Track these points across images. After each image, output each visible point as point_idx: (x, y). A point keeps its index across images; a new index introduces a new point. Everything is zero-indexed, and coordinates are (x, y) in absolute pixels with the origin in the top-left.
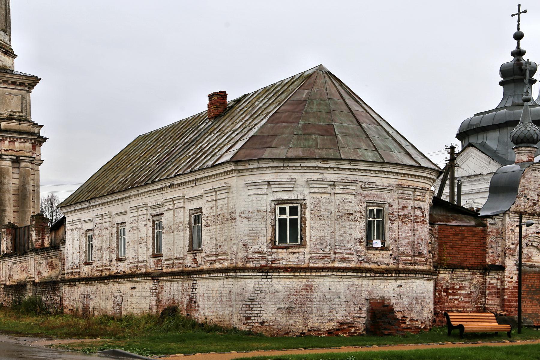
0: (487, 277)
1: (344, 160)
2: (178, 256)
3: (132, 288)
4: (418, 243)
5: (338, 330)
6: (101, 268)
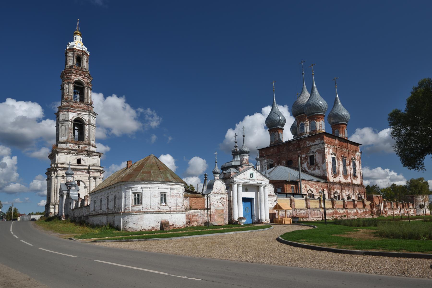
0: (205, 211)
1: (152, 181)
4: (178, 203)
5: (152, 229)
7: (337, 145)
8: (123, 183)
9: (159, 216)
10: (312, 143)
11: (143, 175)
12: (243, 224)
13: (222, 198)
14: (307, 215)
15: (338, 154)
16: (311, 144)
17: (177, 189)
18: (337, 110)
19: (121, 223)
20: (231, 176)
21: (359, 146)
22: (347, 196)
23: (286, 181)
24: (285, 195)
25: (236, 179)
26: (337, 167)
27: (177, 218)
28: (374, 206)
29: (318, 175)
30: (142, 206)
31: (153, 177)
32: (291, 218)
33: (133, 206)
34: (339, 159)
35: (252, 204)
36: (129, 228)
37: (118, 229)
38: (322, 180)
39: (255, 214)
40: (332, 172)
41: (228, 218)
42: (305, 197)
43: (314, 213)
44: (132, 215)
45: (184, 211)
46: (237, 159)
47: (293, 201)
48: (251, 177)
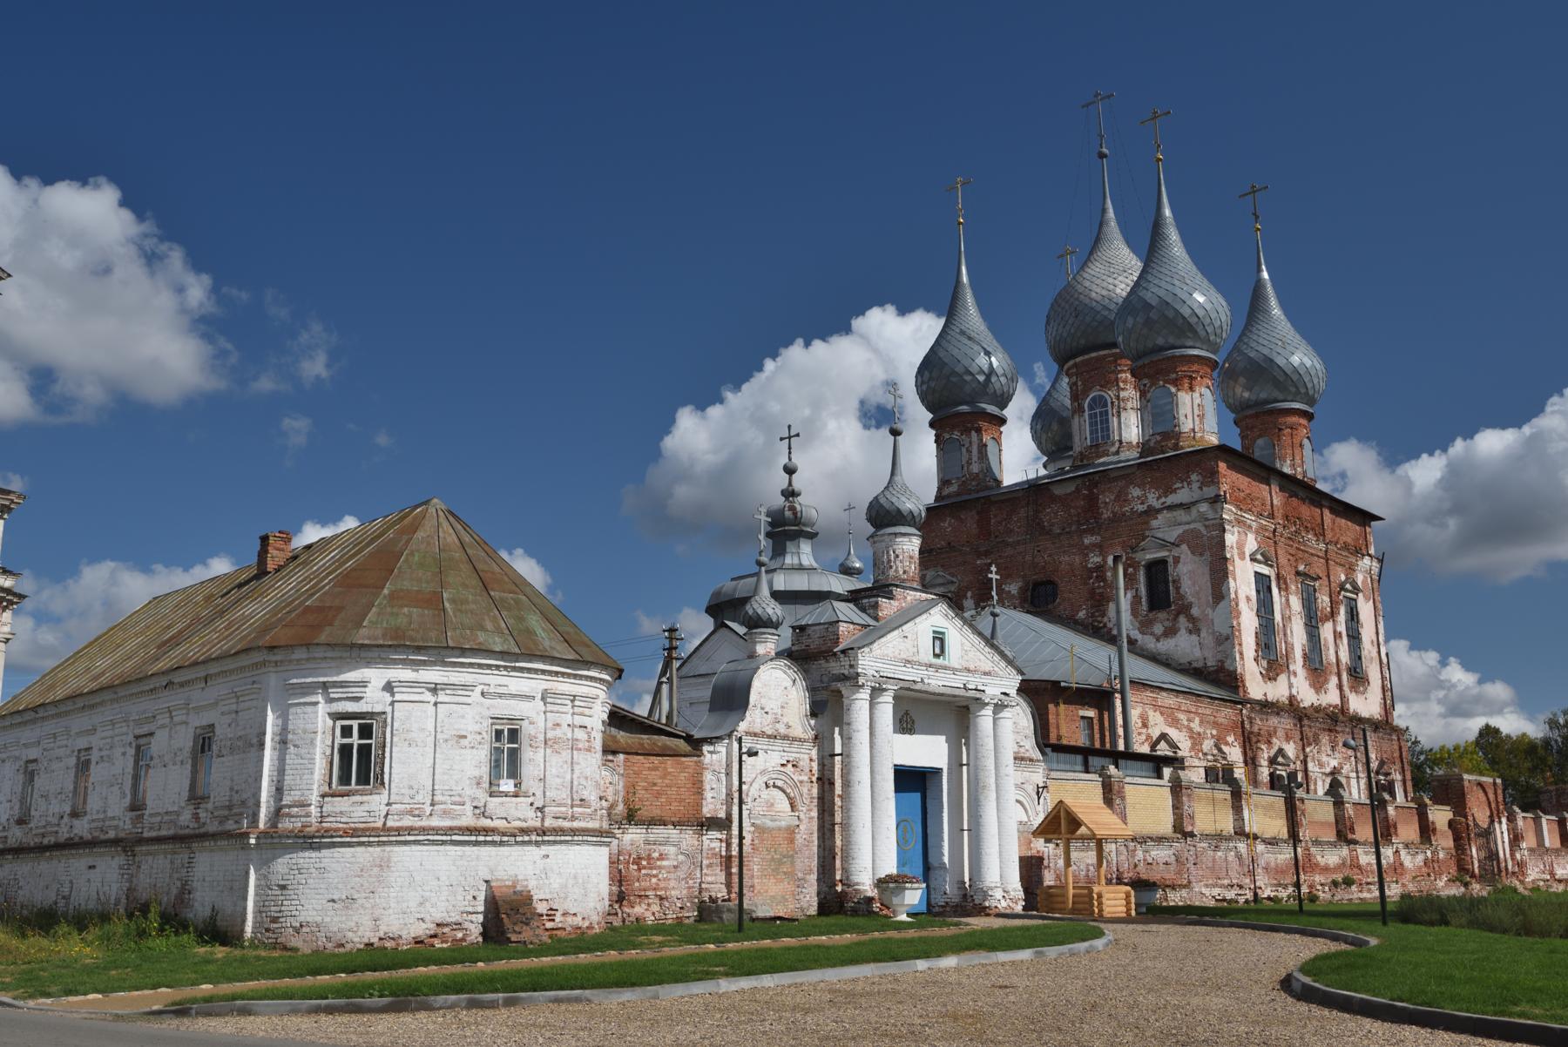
0: (704, 837)
1: (453, 648)
2: (170, 809)
3: (90, 867)
4: (579, 784)
5: (435, 936)
6: (43, 830)
7: (1279, 514)
8: (278, 658)
9: (478, 858)
10: (1158, 499)
11: (395, 610)
12: (908, 915)
13: (790, 765)
14: (1179, 873)
15: (1283, 560)
16: (1153, 499)
17: (577, 703)
18: (1265, 343)
19: (245, 899)
20: (837, 642)
21: (1370, 526)
22: (1327, 775)
23: (1056, 683)
24: (1079, 758)
25: (870, 662)
26: (1281, 625)
27: (573, 871)
28: (1469, 835)
29: (1190, 663)
30: (384, 798)
31: (455, 629)
32: (1129, 888)
33: (333, 796)
34: (1286, 583)
35: (928, 806)
36: (297, 931)
37: (220, 932)
38: (1215, 692)
39: (946, 859)
40: (1256, 651)
41: (818, 880)
42: (1167, 772)
43: (1214, 860)
44: (319, 847)
45: (600, 833)
46: (796, 561)
47: (1119, 792)
48: (936, 656)
